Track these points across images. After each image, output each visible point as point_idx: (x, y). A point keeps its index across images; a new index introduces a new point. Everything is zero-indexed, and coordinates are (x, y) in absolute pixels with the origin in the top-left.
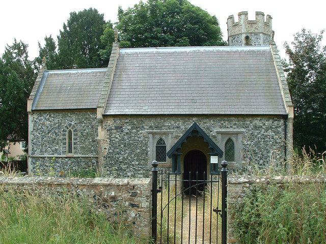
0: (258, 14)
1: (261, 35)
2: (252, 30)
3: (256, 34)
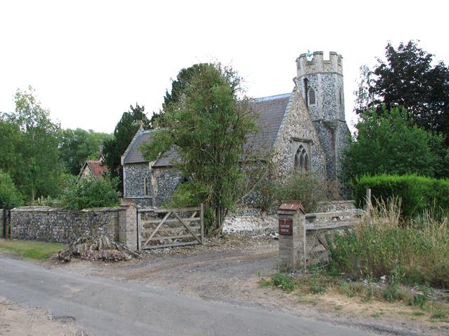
0: (332, 54)
1: (319, 75)
2: (311, 71)
3: (314, 75)
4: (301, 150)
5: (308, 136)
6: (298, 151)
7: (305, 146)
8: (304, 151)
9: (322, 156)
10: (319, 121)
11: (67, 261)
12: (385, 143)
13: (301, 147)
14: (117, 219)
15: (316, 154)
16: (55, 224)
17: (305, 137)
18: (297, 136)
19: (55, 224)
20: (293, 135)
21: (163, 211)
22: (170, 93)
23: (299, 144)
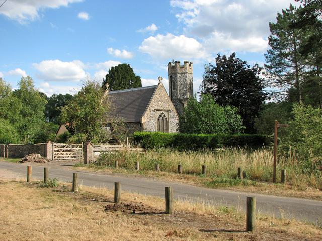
0: (185, 62)
3: (175, 74)
4: (162, 116)
5: (167, 108)
6: (160, 116)
7: (165, 113)
8: (164, 116)
9: (11, 188)
10: (177, 99)
11: (23, 162)
12: (278, 116)
13: (162, 114)
14: (45, 147)
15: (173, 118)
16: (25, 150)
17: (165, 109)
18: (159, 108)
19: (25, 150)
20: (156, 108)
21: (64, 144)
22: (105, 79)
23: (161, 112)
